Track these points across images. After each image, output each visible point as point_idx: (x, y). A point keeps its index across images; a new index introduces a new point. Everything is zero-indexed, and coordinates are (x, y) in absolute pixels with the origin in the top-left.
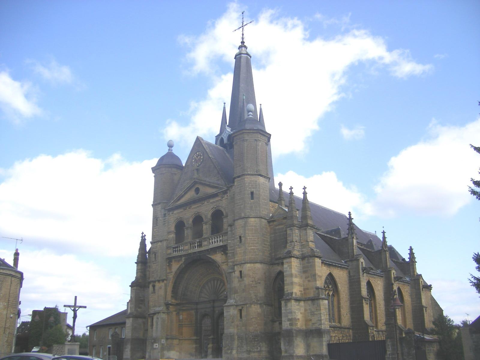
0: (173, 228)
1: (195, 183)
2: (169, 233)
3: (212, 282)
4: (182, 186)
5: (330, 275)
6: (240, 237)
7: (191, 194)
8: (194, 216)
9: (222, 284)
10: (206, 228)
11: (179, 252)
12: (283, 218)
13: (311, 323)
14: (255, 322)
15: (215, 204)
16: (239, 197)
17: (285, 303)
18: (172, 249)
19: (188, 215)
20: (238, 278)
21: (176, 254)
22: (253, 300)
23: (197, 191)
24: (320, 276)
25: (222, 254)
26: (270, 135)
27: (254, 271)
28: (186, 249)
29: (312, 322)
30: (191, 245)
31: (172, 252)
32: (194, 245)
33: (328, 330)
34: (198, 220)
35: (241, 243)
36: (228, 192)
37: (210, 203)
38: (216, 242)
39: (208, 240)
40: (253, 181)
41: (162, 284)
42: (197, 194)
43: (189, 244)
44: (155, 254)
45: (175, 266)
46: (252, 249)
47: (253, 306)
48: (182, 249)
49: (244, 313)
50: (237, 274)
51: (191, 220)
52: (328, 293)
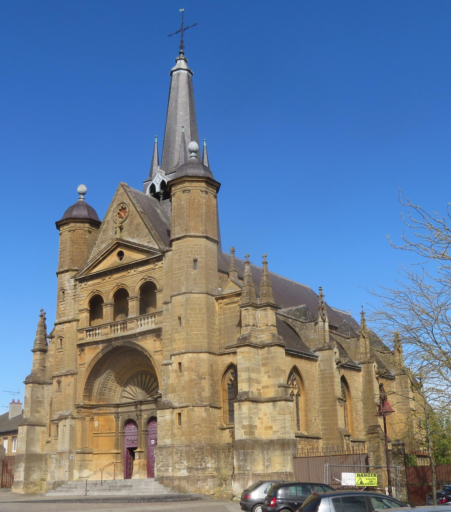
0: (86, 305)
1: (118, 245)
2: (81, 311)
3: (139, 377)
4: (99, 249)
5: (295, 370)
6: (180, 318)
7: (112, 260)
8: (115, 290)
9: (152, 380)
10: (133, 305)
11: (94, 337)
12: (236, 294)
13: (272, 431)
14: (199, 429)
15: (144, 274)
16: (178, 265)
17: (240, 405)
18: (85, 332)
19: (107, 288)
20: (176, 372)
21: (89, 339)
22: (196, 401)
23: (121, 255)
24: (284, 370)
25: (155, 340)
26: (220, 184)
27: (197, 363)
28: (103, 334)
29: (274, 430)
30: (111, 327)
31: (85, 337)
32: (116, 327)
33: (293, 440)
34: (121, 295)
35: (180, 326)
36: (164, 259)
37: (112, 279)
38: (148, 324)
39: (135, 321)
40: (197, 245)
41: (70, 379)
42: (121, 259)
43: (109, 327)
44: (61, 340)
45: (90, 355)
46: (195, 334)
47: (196, 409)
48: (99, 333)
49: (183, 419)
50: (175, 366)
51: (112, 294)
52: (292, 392)
